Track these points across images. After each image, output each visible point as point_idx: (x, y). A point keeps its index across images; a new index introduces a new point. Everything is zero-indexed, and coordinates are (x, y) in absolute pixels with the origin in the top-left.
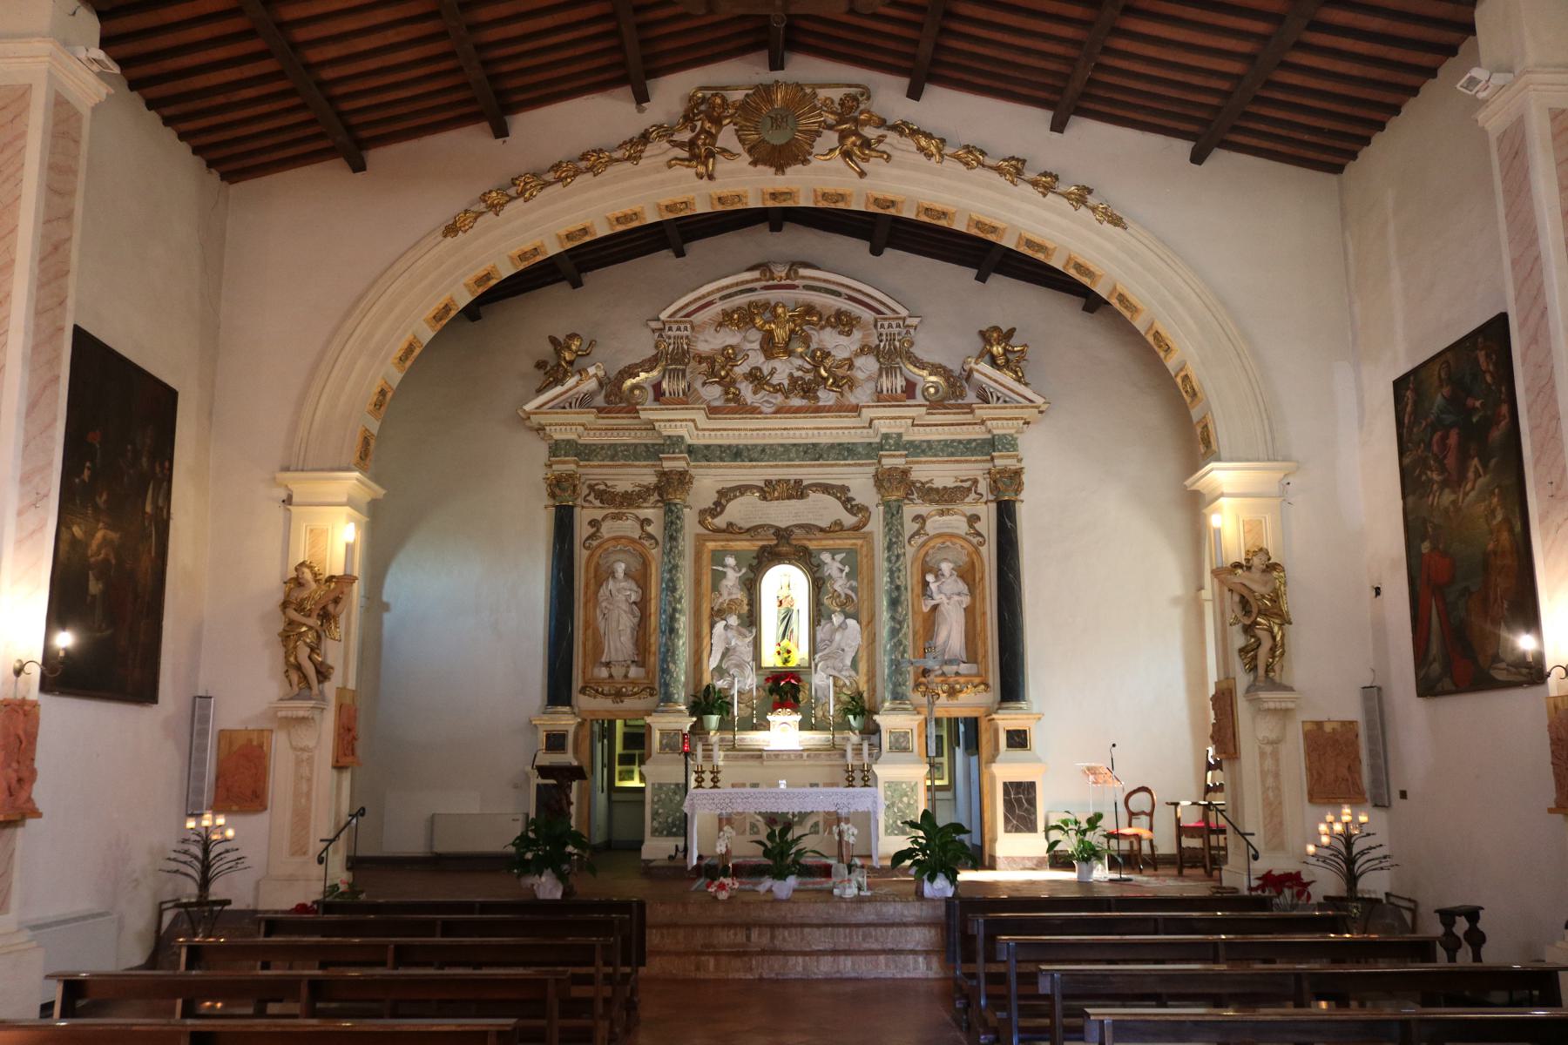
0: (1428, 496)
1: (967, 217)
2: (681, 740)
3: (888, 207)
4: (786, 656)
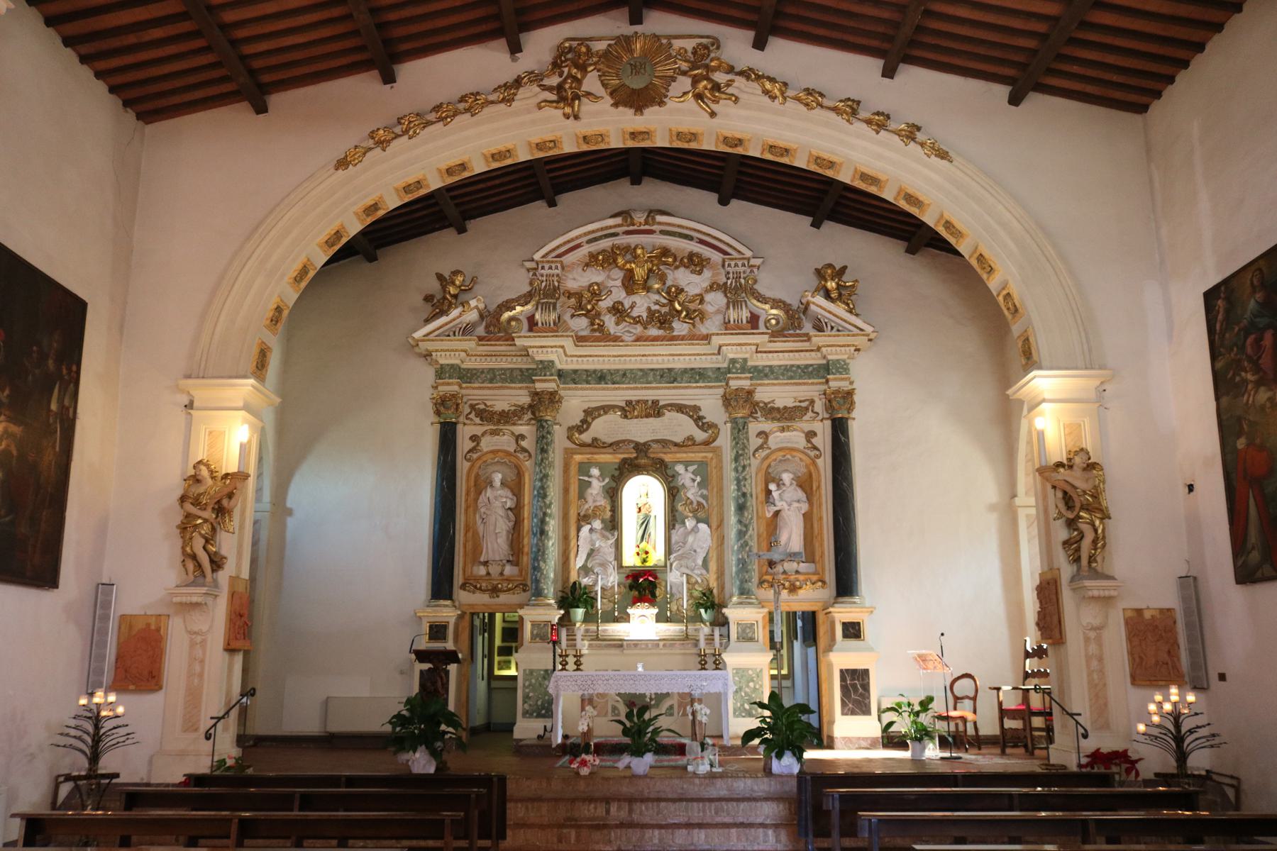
0: (1243, 395)
1: (807, 154)
2: (550, 630)
3: (736, 146)
4: (644, 556)
